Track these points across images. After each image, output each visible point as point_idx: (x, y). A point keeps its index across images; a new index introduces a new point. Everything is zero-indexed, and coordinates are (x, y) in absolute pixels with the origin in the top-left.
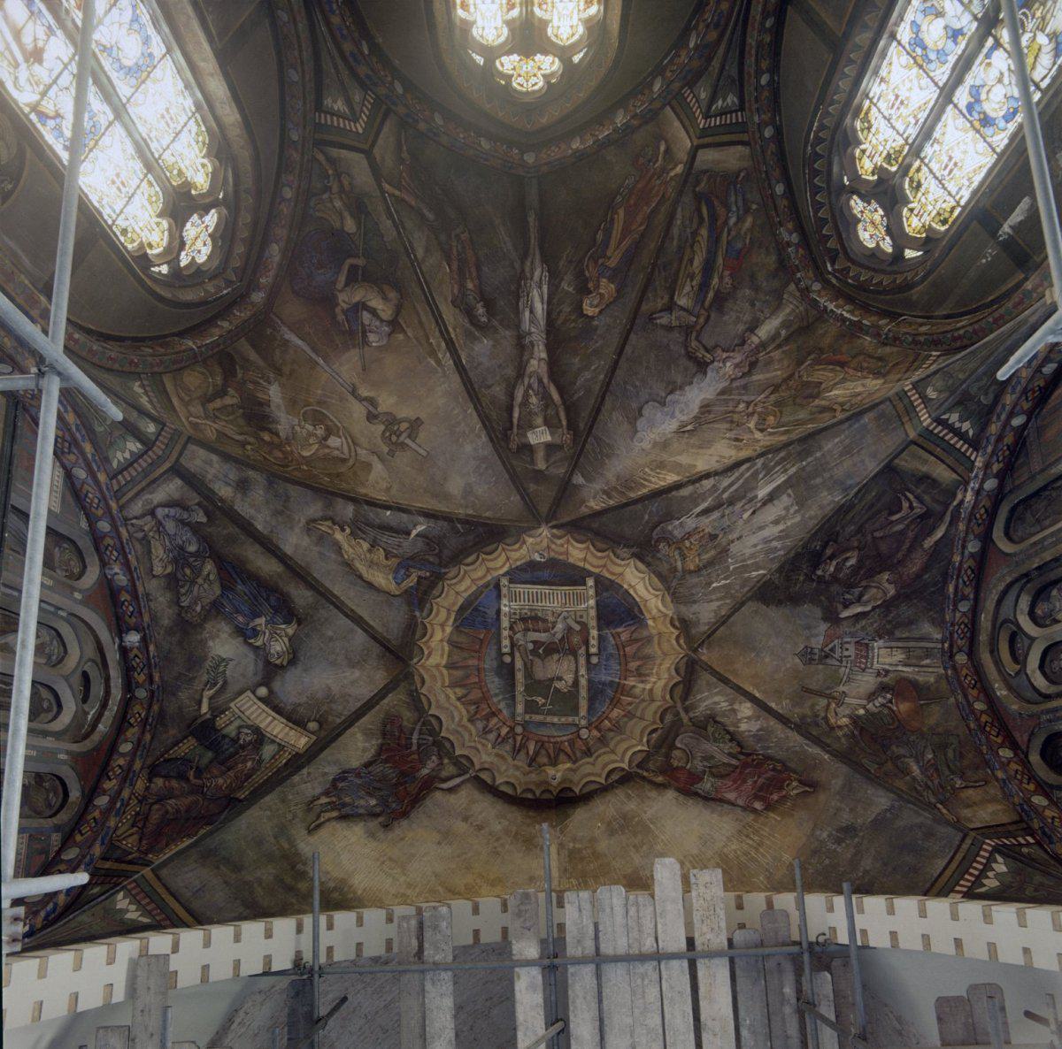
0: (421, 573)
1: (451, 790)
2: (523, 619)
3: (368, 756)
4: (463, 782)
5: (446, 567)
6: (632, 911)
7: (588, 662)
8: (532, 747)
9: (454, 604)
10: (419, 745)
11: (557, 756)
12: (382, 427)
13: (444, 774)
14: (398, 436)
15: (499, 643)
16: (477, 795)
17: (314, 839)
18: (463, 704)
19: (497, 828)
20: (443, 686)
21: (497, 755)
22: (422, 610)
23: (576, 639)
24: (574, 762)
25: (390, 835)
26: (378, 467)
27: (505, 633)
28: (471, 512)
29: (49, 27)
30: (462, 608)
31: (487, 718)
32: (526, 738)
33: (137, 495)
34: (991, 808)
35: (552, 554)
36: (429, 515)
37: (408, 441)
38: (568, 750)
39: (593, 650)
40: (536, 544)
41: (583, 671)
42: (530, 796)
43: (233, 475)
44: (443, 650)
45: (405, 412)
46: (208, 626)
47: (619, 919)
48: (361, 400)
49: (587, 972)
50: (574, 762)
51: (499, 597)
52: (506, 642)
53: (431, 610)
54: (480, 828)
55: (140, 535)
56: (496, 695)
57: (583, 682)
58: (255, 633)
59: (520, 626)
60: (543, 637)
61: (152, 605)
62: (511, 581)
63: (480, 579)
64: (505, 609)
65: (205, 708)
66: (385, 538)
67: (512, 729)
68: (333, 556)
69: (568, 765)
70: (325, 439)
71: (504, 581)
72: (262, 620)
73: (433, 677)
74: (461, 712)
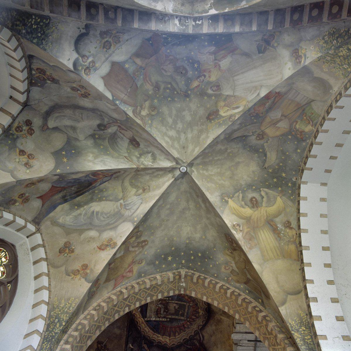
1: (203, 337)
2: (157, 314)
6: (244, 345)
7: (170, 300)
8: (193, 317)
9: (152, 333)
10: (191, 346)
11: (197, 312)
13: (199, 338)
14: (102, 347)
15: (163, 321)
18: (180, 333)
19: (214, 327)
23: (164, 302)
24: (199, 308)
27: (161, 319)
28: (125, 329)
30: (153, 331)
31: (185, 328)
32: (191, 318)
34: (239, 348)
41: (174, 302)
42: (207, 317)
44: (165, 338)
51: (151, 321)
52: (163, 319)
53: (154, 340)
54: (214, 333)
56: (178, 324)
57: (176, 302)
59: (159, 315)
62: (146, 317)
64: (154, 319)
67: (188, 321)
71: (146, 319)
73: (173, 341)
74: (183, 334)
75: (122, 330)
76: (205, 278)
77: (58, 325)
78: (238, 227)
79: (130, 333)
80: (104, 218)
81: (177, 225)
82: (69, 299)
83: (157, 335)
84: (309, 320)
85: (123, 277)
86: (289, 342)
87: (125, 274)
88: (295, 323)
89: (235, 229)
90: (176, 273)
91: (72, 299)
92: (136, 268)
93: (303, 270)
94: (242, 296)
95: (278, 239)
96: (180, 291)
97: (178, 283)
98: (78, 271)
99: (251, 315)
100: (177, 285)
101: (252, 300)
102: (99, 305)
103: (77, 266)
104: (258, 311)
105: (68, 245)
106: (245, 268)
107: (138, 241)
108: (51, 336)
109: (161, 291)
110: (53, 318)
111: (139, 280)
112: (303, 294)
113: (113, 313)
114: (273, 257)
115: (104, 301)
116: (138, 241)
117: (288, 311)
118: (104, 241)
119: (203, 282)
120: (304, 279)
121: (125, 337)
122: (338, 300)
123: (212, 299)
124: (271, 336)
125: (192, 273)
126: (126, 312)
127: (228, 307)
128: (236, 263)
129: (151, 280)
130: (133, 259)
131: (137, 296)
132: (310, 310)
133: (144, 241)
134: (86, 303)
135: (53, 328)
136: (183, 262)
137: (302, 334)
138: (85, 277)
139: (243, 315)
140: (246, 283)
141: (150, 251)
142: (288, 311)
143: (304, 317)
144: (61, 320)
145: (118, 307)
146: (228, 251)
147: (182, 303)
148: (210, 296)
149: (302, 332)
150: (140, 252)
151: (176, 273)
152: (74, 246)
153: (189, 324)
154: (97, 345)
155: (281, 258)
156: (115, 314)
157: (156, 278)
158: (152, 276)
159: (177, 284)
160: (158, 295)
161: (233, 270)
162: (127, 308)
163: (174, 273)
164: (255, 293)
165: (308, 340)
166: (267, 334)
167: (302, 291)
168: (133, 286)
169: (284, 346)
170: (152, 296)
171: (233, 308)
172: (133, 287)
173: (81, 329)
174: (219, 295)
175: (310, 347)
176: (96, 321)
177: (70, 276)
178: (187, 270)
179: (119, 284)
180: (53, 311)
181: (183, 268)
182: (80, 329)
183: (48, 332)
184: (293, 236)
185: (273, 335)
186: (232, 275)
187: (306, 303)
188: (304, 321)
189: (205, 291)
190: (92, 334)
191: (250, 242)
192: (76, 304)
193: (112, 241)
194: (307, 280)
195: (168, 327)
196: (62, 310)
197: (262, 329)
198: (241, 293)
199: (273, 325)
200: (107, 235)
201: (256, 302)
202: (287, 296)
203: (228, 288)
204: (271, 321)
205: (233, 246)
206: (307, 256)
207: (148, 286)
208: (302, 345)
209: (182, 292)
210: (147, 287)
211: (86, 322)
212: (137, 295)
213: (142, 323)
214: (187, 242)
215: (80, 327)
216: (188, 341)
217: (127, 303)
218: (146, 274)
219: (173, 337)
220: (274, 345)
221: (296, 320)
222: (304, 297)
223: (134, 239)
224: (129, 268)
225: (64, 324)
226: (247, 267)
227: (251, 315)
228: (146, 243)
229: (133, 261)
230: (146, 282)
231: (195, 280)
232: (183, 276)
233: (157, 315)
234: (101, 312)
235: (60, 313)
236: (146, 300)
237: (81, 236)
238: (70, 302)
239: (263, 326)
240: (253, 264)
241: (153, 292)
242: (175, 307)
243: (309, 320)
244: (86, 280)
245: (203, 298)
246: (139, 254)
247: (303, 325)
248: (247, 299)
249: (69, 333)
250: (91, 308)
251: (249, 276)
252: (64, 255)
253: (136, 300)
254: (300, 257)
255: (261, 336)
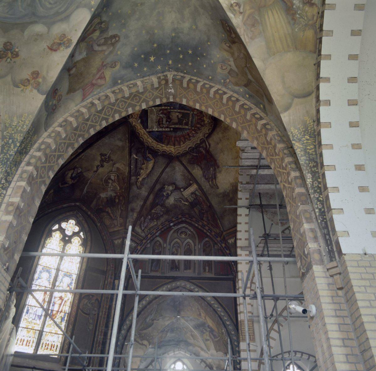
0: (147, 153)
1: (210, 145)
2: (159, 125)
3: (199, 168)
4: (208, 142)
5: (145, 146)
7: (172, 109)
8: (198, 126)
9: (156, 143)
10: (197, 153)
12: (105, 163)
13: (205, 146)
14: (106, 159)
15: (167, 131)
16: (211, 139)
17: (220, 187)
19: (220, 135)
20: (180, 148)
21: (200, 133)
22: (158, 152)
23: (165, 112)
24: (204, 116)
25: (221, 167)
26: (117, 165)
27: (164, 129)
28: (127, 141)
29: (55, 298)
30: (157, 141)
31: (190, 137)
33: (140, 236)
35: (138, 118)
36: (130, 155)
37: (107, 156)
38: (200, 117)
39: (169, 108)
40: (135, 121)
41: (176, 111)
42: (213, 126)
43: (131, 214)
44: (170, 147)
45: (99, 158)
46: (167, 205)
47: (251, 154)
48: (98, 169)
49: (262, 161)
50: (204, 116)
51: (153, 131)
52: (166, 129)
53: (158, 149)
54: (221, 140)
55: (149, 231)
56: (183, 133)
57: (179, 111)
58: (168, 194)
59: (161, 125)
60: (164, 120)
61: (163, 222)
63: (147, 136)
64: (156, 130)
65: (187, 203)
66: (139, 166)
67: (193, 130)
68: (146, 180)
69: (205, 118)
70: (112, 180)
71: (148, 130)
72: (165, 194)
75: (124, 142)
76: (198, 82)
77: (12, 146)
78: (236, 8)
79: (132, 145)
80: (50, 4)
81: (157, 11)
82: (21, 116)
83: (162, 145)
84: (315, 127)
85: (93, 85)
86: (289, 152)
87: (94, 82)
88: (298, 131)
89: (234, 11)
90: (162, 78)
91: (25, 116)
92: (108, 74)
93: (318, 65)
94: (240, 102)
95: (292, 22)
96: (168, 98)
97: (165, 90)
98: (28, 80)
99: (249, 123)
100: (164, 91)
101: (252, 106)
102: (66, 121)
103: (26, 74)
104: (257, 119)
105: (9, 47)
106: (246, 66)
107: (105, 36)
108: (6, 158)
109: (144, 100)
110: (6, 138)
111: (115, 88)
112: (314, 97)
113: (86, 128)
114: (281, 50)
115: (71, 116)
116: (105, 36)
117: (291, 118)
118: (55, 39)
119: (194, 86)
120: (318, 77)
121: (128, 148)
122: (357, 102)
123: (207, 107)
124: (270, 146)
125: (182, 76)
126: (104, 126)
127: (224, 115)
128: (235, 61)
129: (130, 87)
130: (103, 63)
131: (115, 108)
132: (318, 115)
133: (114, 36)
134: (46, 119)
135: (8, 150)
136: (170, 62)
137: (304, 143)
138: (37, 87)
139: (241, 124)
140: (246, 86)
141: (124, 51)
142: (291, 118)
143: (310, 125)
144: (15, 140)
145: (92, 121)
146: (225, 44)
147: (186, 111)
148: (204, 103)
149: (305, 142)
150: (111, 52)
151: (162, 78)
152: (17, 48)
153: (194, 133)
154: (101, 157)
155: (292, 50)
156: (89, 129)
157: (136, 84)
158: (132, 82)
159: (163, 90)
160: (141, 104)
161: (231, 70)
162: (104, 121)
163: (159, 78)
164: (257, 97)
165: (310, 150)
166: (266, 143)
167: (313, 92)
168: (108, 96)
169: (283, 157)
170: (134, 106)
171: (229, 116)
172: (107, 97)
173: (45, 149)
174: (214, 101)
175: (311, 158)
176: (65, 139)
177: (19, 87)
178: (176, 73)
179: (89, 94)
180: (6, 130)
181: (170, 70)
182: (43, 149)
183: (4, 154)
184: (313, 16)
185: (272, 145)
186: (230, 77)
187: (316, 107)
188: (309, 128)
189: (197, 97)
190: (63, 152)
191: (253, 29)
192: (29, 121)
193: (66, 37)
194: (322, 78)
195: (172, 137)
196: (15, 129)
197: (260, 139)
198: (239, 98)
199: (273, 134)
200: (58, 29)
201: (257, 109)
202: (293, 100)
203: (225, 93)
204: (271, 130)
205: (232, 37)
206: (326, 47)
207: (127, 95)
208: (302, 156)
209: (171, 100)
210: (126, 96)
211: (50, 141)
212: (114, 106)
213: (144, 134)
214: (173, 35)
215: (43, 147)
216: (193, 149)
217: (102, 115)
218: (123, 80)
219: (178, 146)
220: (272, 156)
221: (299, 128)
222: (314, 100)
223: (97, 33)
224: (99, 74)
225: (18, 145)
226: (248, 65)
227: (249, 123)
228: (117, 39)
229: (102, 64)
230: (123, 90)
231: (185, 85)
232: (170, 81)
233: (159, 125)
234: (69, 128)
235: (13, 132)
236: (127, 111)
237: (23, 32)
238: (23, 119)
239: (262, 135)
240: (254, 59)
241: (135, 101)
242: (178, 116)
243: (315, 127)
244: (38, 91)
245: (196, 105)
246: (109, 54)
247: (307, 134)
248: (246, 104)
249: (30, 153)
250: (56, 124)
251: (250, 77)
252: (6, 60)
253: (114, 112)
254: (318, 47)
255: (259, 146)
